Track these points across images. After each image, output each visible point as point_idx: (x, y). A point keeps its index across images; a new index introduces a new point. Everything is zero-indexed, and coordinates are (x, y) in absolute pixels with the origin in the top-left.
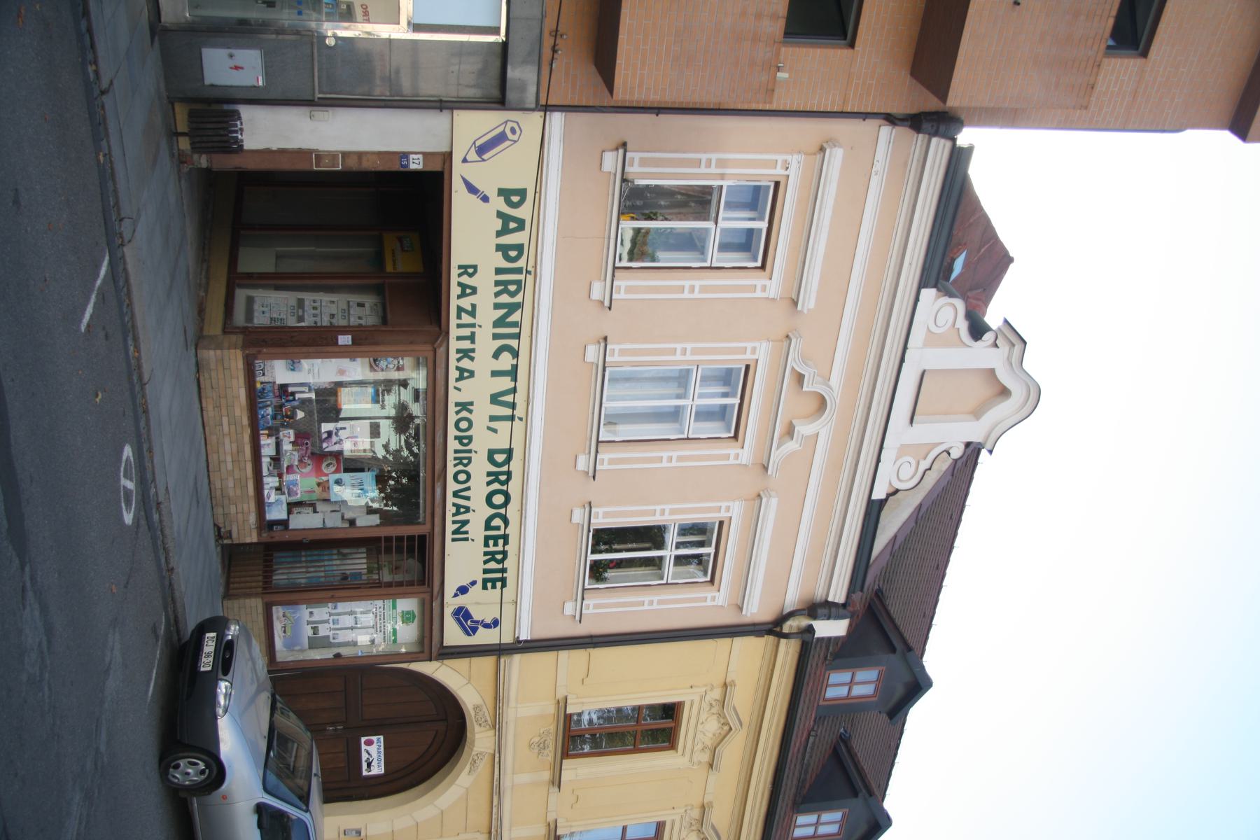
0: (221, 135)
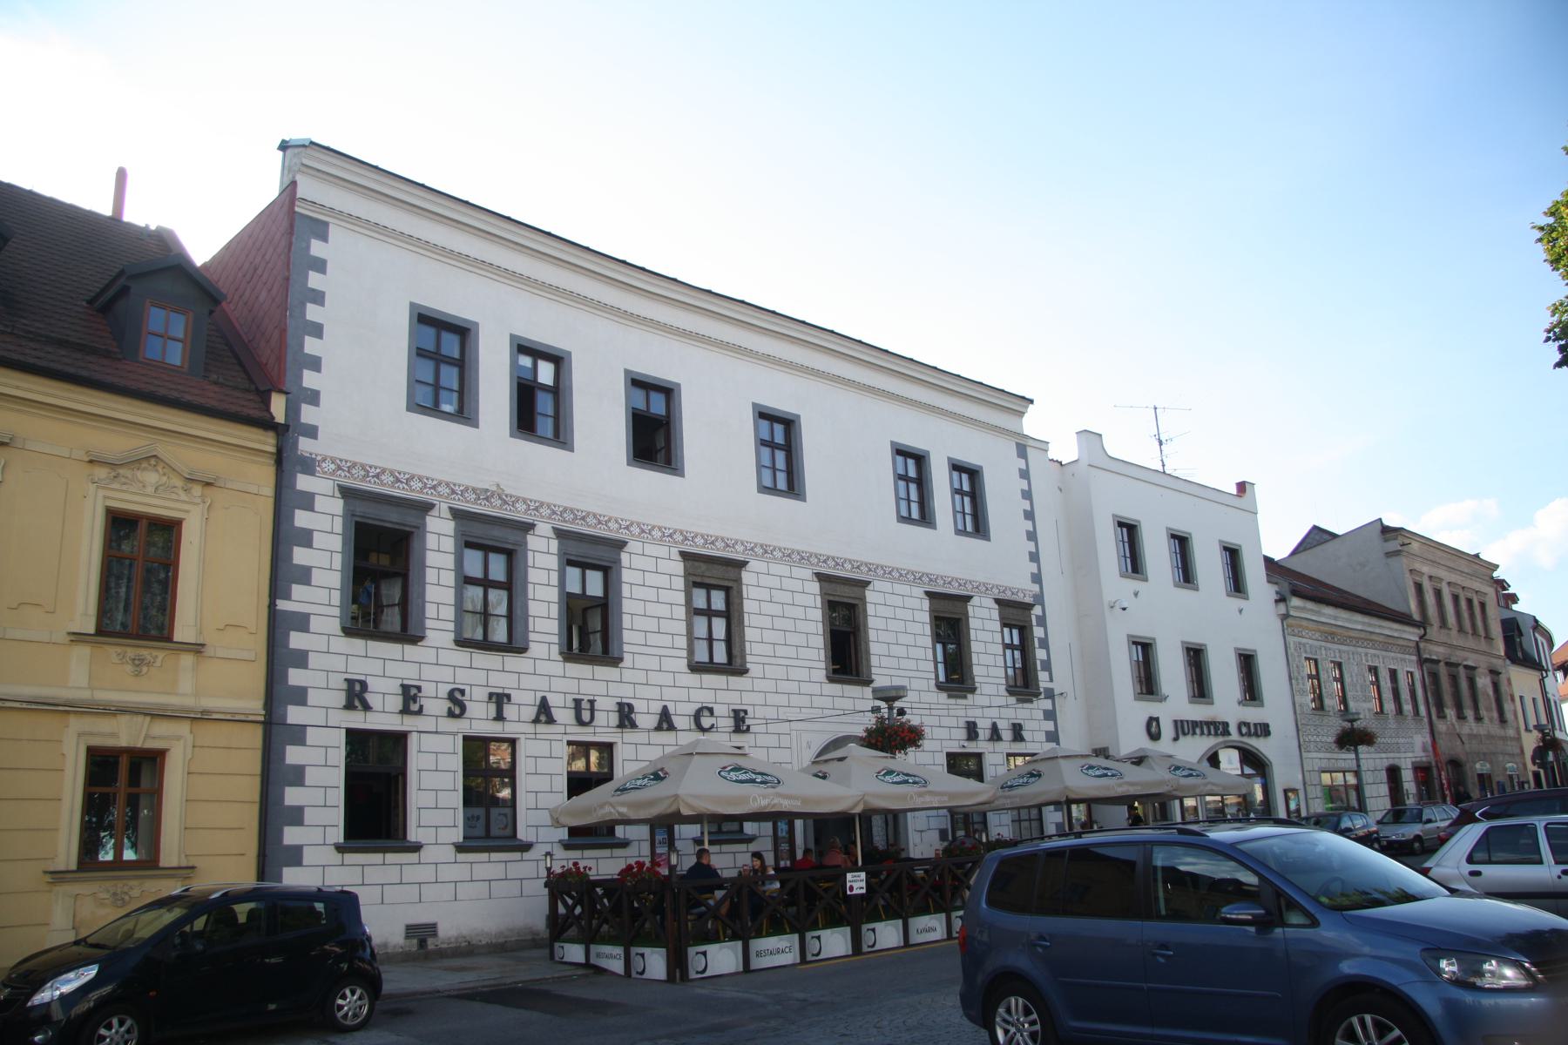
0: (1476, 708)
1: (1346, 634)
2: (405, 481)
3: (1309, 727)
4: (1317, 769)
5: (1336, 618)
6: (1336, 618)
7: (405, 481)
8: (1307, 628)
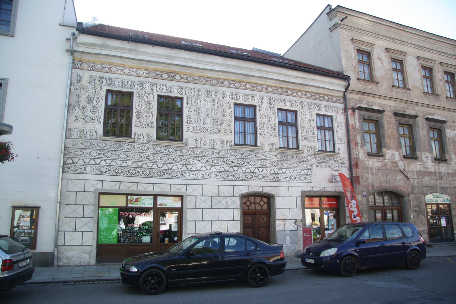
1: (200, 74)
2: (242, 86)
3: (88, 151)
4: (92, 189)
5: (169, 57)
6: (169, 57)
7: (242, 86)
8: (121, 65)
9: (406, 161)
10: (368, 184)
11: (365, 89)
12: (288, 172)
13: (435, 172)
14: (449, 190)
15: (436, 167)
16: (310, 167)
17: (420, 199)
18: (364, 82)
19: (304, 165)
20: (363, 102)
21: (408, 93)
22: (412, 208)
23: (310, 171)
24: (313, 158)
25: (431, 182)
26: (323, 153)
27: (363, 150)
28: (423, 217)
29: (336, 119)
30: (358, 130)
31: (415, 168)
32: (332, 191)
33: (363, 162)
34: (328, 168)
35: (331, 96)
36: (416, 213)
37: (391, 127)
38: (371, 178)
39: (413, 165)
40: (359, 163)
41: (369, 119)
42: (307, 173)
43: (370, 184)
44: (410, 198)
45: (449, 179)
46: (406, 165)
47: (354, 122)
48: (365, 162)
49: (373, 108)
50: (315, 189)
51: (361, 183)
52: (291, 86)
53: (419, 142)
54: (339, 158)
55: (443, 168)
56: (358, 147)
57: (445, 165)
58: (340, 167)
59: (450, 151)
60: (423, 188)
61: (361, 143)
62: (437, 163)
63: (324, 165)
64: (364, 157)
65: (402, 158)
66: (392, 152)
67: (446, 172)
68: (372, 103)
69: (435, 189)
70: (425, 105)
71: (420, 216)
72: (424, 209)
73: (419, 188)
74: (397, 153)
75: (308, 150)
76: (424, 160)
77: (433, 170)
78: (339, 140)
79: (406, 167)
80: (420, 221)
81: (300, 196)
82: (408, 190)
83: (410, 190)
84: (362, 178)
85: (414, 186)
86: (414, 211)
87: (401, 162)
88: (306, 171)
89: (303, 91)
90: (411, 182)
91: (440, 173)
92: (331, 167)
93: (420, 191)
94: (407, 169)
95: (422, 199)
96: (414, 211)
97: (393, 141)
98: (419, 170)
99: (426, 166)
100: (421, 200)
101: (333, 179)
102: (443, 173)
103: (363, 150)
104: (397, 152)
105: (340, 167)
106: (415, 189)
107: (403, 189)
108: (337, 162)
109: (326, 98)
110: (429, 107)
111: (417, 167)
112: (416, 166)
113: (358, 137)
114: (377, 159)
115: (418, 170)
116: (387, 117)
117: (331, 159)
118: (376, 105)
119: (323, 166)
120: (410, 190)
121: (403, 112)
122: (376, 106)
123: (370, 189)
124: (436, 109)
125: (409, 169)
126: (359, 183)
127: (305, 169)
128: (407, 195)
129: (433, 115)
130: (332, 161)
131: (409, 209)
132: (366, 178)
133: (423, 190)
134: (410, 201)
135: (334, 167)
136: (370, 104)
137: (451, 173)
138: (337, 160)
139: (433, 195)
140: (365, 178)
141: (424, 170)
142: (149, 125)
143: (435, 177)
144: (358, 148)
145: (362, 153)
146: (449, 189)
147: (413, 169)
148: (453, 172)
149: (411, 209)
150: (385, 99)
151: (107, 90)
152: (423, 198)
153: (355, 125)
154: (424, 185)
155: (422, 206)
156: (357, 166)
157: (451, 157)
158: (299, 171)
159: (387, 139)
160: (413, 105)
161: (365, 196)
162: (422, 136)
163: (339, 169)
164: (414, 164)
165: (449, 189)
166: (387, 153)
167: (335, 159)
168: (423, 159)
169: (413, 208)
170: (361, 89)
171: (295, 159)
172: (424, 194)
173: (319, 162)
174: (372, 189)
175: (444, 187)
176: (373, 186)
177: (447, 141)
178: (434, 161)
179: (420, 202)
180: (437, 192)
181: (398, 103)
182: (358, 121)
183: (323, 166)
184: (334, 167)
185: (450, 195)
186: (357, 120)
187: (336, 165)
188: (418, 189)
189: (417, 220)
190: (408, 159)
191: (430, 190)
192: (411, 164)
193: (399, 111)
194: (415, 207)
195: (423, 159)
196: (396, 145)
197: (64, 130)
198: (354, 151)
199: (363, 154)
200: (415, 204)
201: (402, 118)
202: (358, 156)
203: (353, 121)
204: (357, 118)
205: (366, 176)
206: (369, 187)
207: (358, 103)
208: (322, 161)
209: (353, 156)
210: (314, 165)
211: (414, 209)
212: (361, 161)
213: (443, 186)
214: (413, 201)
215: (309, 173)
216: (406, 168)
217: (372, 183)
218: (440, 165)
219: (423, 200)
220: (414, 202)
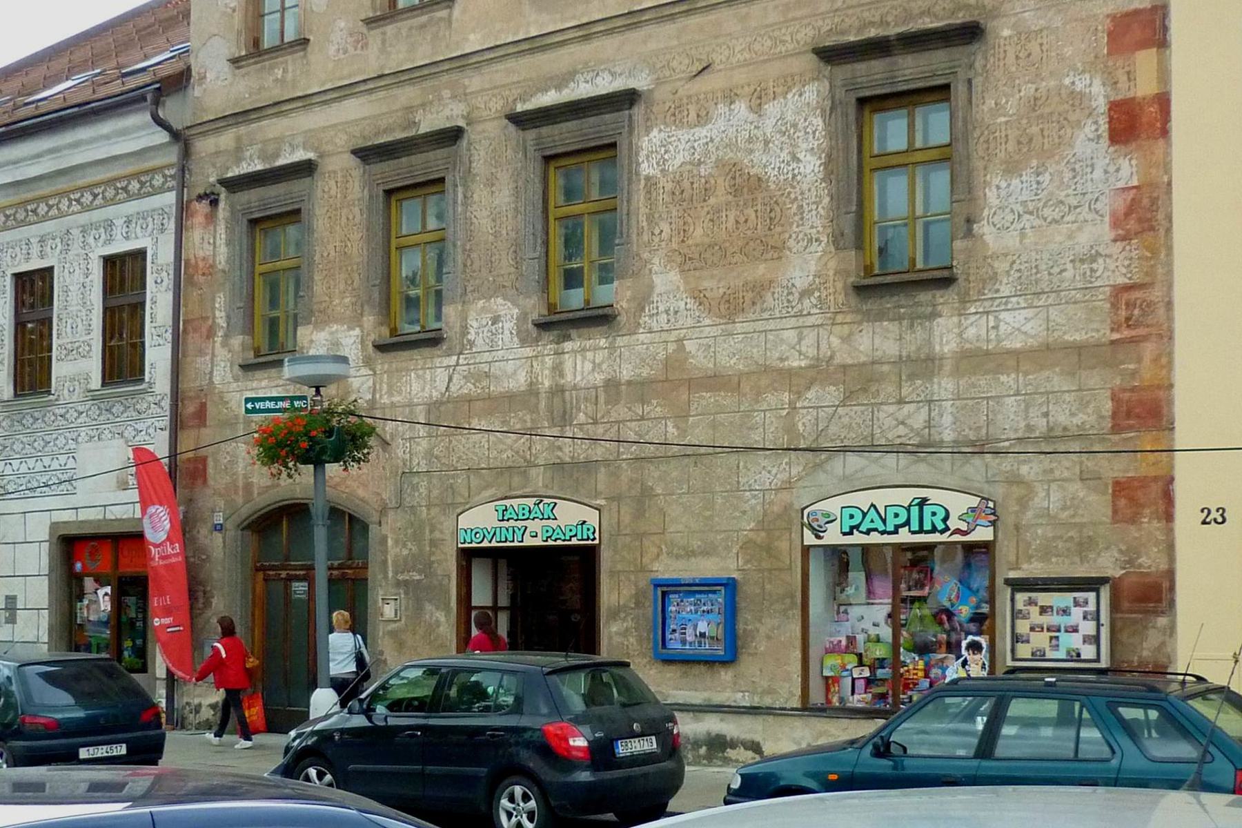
9: (384, 363)
10: (234, 482)
11: (261, 88)
12: (24, 469)
13: (532, 389)
14: (602, 475)
15: (543, 362)
16: (72, 445)
17: (431, 532)
18: (256, 63)
19: (57, 442)
20: (248, 154)
21: (441, 19)
22: (390, 574)
23: (73, 457)
24: (82, 413)
25: (501, 446)
26: (137, 388)
27: (229, 351)
28: (440, 616)
29: (155, 255)
30: (220, 274)
31: (423, 390)
32: (124, 517)
33: (221, 398)
34: (119, 442)
35: (146, 172)
36: (406, 593)
37: (344, 220)
38: (244, 459)
39: (418, 377)
40: (209, 404)
41: (268, 213)
42: (65, 465)
43: (240, 484)
44: (385, 530)
45: (614, 416)
46: (382, 381)
47: (212, 248)
48: (227, 397)
49: (281, 162)
50: (84, 515)
51: (211, 482)
52: (45, 189)
53: (460, 258)
54: (151, 399)
55: (584, 358)
56: (214, 342)
57: (603, 342)
58: (151, 431)
59: (645, 255)
60: (453, 477)
61: (225, 325)
62: (551, 342)
63: (106, 432)
64: (229, 377)
65: (370, 348)
66: (332, 333)
67: (599, 378)
68: (279, 140)
69: (516, 480)
70: (511, 50)
71: (429, 607)
72: (449, 577)
73: (435, 481)
74: (351, 333)
75: (71, 389)
76: (479, 341)
77: (519, 382)
78: (155, 333)
79: (381, 390)
80: (421, 631)
81: (47, 538)
82: (379, 494)
83: (388, 494)
84: (216, 461)
85: (409, 474)
86: (398, 584)
87: (364, 371)
88: (63, 459)
89: (72, 191)
90: (400, 454)
91: (558, 391)
92: (126, 434)
93: (435, 493)
94: (385, 400)
95: (442, 532)
96: (398, 584)
97: (342, 287)
98: (443, 395)
99: (486, 368)
100: (437, 535)
101: (130, 477)
102: (575, 387)
103: (229, 351)
104: (353, 329)
105: (151, 431)
106: (415, 488)
107: (361, 492)
108: (142, 416)
109: (134, 186)
110: (544, 48)
111: (433, 380)
112: (428, 377)
113: (217, 305)
114: (269, 378)
115: (435, 394)
116: (332, 183)
117: (127, 408)
118: (296, 142)
119: (103, 436)
120: (388, 494)
121: (405, 129)
122: (293, 148)
123: (240, 500)
124: (586, 38)
125: (396, 399)
126: (205, 481)
127: (62, 452)
128: (375, 518)
129: (561, 82)
130: (132, 413)
131: (380, 577)
132: (228, 458)
133: (451, 486)
134: (384, 540)
135: (134, 433)
136: (271, 148)
137: (629, 383)
138: (145, 405)
139: (501, 509)
140: (225, 460)
141: (468, 388)
142: (64, 352)
143: (528, 417)
144: (213, 348)
145: (223, 364)
146: (603, 469)
147: (414, 393)
148: (645, 372)
149: (386, 577)
150: (325, 102)
151: (384, 191)
152: (448, 525)
153: (214, 261)
154: (459, 466)
155: (439, 562)
156: (201, 415)
157: (651, 287)
158: (47, 461)
159: (320, 283)
160: (454, 76)
161: (218, 527)
162: (482, 221)
163: (147, 438)
164: (420, 372)
165: (603, 469)
166: (312, 341)
167: (138, 406)
168: (471, 337)
169: (396, 573)
170: (245, 98)
171: (39, 424)
172: (454, 505)
173: (94, 423)
174: (246, 503)
175: (575, 464)
176: (248, 487)
177: (640, 199)
178: (534, 332)
179: (433, 543)
180: (528, 490)
181: (381, 94)
182: (223, 241)
183: (103, 436)
184: (134, 433)
185: (600, 502)
186: (223, 236)
187: (140, 426)
188: (430, 482)
189: (410, 628)
190: (393, 354)
191: (486, 488)
192: (408, 370)
193: (385, 131)
194: (404, 565)
195: (471, 337)
196: (354, 300)
197: (917, 229)
198: (197, 365)
199: (228, 369)
200: (405, 552)
201: (396, 161)
202: (211, 378)
203: (209, 243)
204: (221, 229)
205: (228, 453)
206: (236, 493)
207: (229, 164)
208: (102, 418)
209: (190, 384)
210: (83, 434)
211: (401, 577)
212: (216, 398)
213: (568, 459)
214: (396, 542)
215: (71, 464)
216: (381, 397)
217: (245, 477)
218: (568, 346)
219: (448, 537)
220: (405, 545)
